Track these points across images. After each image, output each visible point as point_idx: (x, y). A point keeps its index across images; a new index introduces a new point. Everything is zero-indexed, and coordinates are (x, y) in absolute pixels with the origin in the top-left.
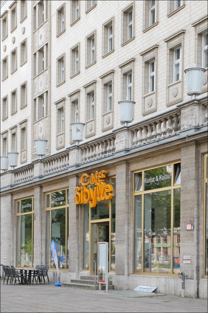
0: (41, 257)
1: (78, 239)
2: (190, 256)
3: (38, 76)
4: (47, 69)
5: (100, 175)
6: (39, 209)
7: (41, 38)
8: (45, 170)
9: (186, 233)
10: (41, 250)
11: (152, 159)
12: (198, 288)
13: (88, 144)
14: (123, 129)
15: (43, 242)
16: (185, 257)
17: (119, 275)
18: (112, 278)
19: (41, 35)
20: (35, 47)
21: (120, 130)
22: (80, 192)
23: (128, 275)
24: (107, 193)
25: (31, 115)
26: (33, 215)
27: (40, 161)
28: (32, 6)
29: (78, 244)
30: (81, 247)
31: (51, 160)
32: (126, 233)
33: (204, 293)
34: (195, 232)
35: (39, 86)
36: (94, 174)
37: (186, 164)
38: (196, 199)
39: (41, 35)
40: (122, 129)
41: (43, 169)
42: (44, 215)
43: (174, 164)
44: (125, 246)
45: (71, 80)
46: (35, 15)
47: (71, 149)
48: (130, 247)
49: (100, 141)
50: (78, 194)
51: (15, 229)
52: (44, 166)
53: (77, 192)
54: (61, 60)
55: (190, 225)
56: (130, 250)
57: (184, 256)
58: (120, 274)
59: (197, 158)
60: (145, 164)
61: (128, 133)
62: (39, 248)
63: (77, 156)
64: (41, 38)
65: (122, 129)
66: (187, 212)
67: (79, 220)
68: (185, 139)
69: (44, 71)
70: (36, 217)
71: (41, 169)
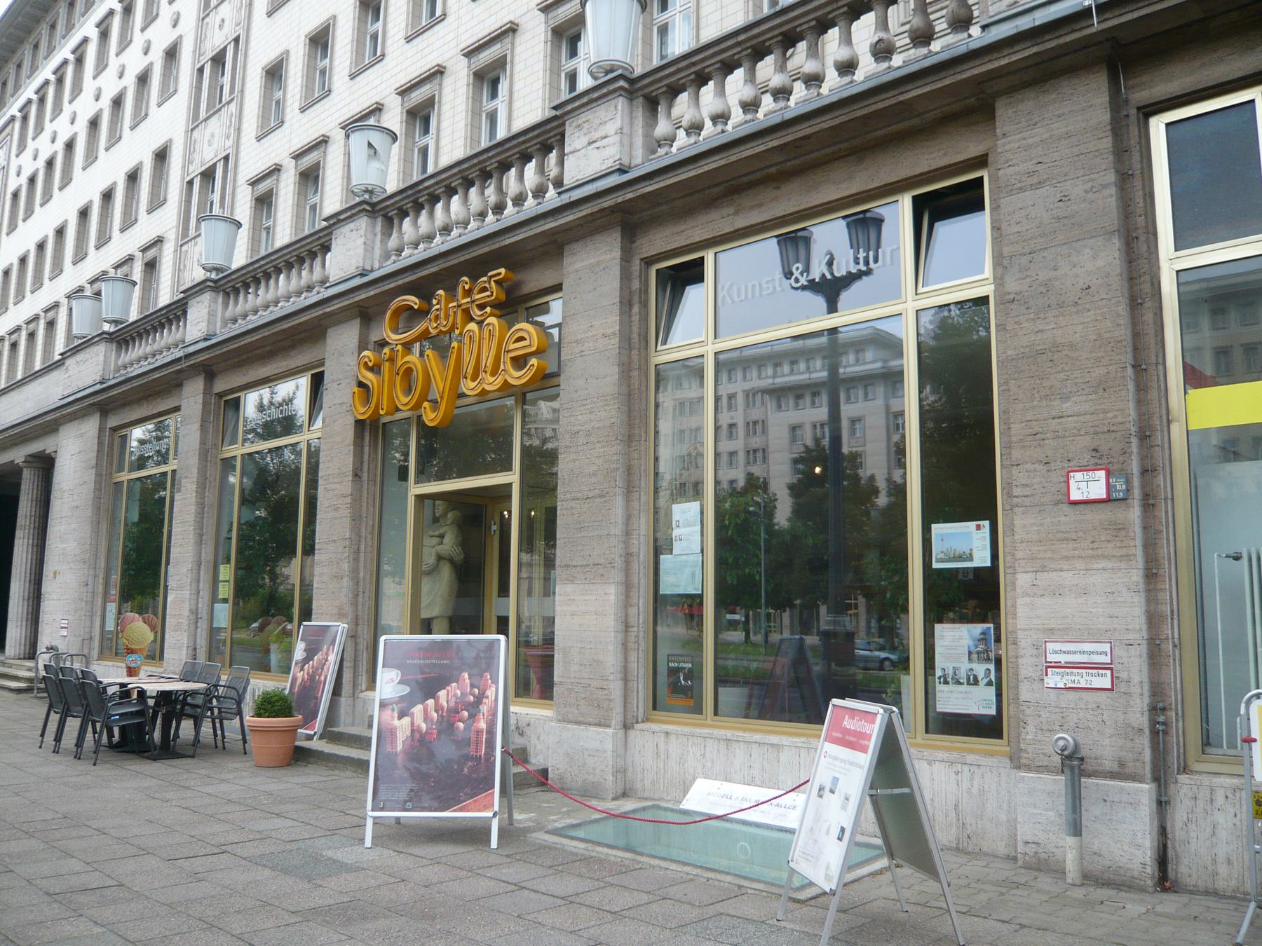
0: (193, 627)
1: (356, 560)
2: (1106, 647)
3: (205, 120)
4: (233, 99)
5: (484, 290)
6: (197, 452)
7: (221, 27)
8: (229, 313)
9: (1063, 519)
10: (193, 602)
11: (778, 188)
12: (1163, 831)
13: (421, 187)
14: (612, 87)
15: (202, 573)
16: (1055, 652)
17: (578, 723)
18: (528, 731)
19: (223, 20)
20: (202, 51)
21: (596, 95)
22: (377, 369)
23: (626, 727)
24: (519, 362)
25: (175, 223)
26: (173, 479)
27: (211, 284)
28: (183, 178)
29: (1175, 851)
30: (367, 594)
31: (254, 277)
32: (617, 530)
33: (1214, 861)
34: (1134, 513)
35: (206, 146)
36: (451, 291)
37: (1040, 167)
38: (1124, 333)
39: (223, 20)
40: (605, 90)
41: (219, 314)
42: (214, 472)
43: (914, 198)
44: (612, 589)
45: (303, 115)
46: (199, 88)
47: (342, 217)
48: (634, 594)
49: (477, 168)
50: (369, 378)
51: (104, 527)
52: (226, 305)
53: (363, 370)
54: (275, 73)
55: (1102, 474)
56: (633, 611)
57: (1050, 646)
58: (581, 719)
59: (1118, 127)
60: (734, 214)
61: (631, 105)
62: (187, 593)
63: (368, 242)
64: (221, 27)
65: (605, 90)
66: (1067, 407)
67: (362, 486)
68: (1084, 24)
69: (224, 106)
70: (183, 481)
71: (211, 314)
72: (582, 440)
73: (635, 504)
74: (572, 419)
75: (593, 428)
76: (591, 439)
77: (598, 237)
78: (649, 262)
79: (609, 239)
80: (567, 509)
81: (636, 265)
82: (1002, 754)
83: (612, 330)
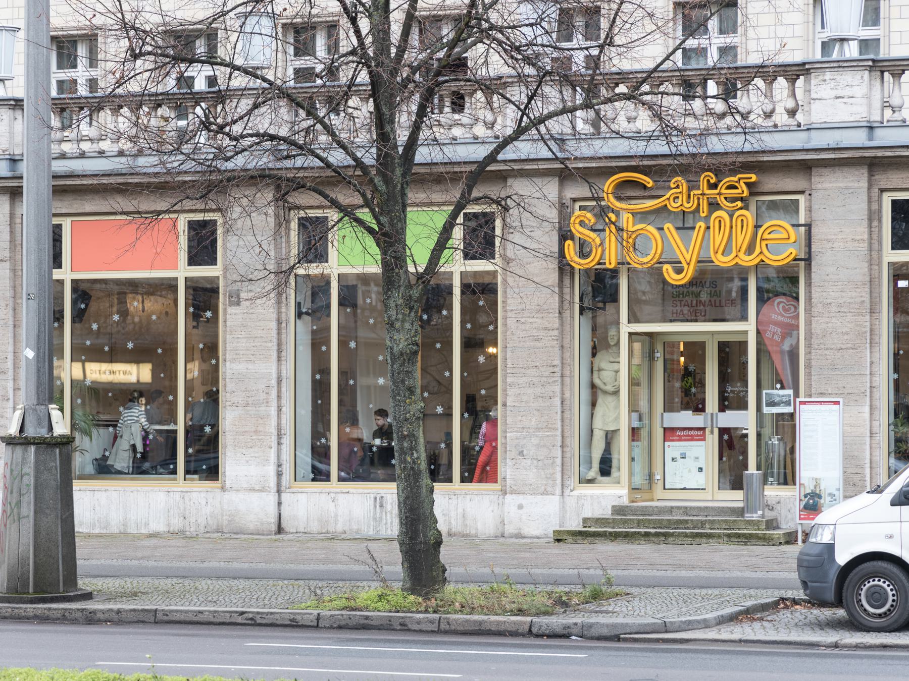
18: (778, 507)
72: (834, 309)
73: (877, 355)
74: (824, 294)
75: (845, 302)
76: (843, 309)
77: (846, 169)
78: (882, 191)
79: (857, 173)
80: (822, 355)
81: (875, 191)
82: (217, 488)
83: (862, 237)
